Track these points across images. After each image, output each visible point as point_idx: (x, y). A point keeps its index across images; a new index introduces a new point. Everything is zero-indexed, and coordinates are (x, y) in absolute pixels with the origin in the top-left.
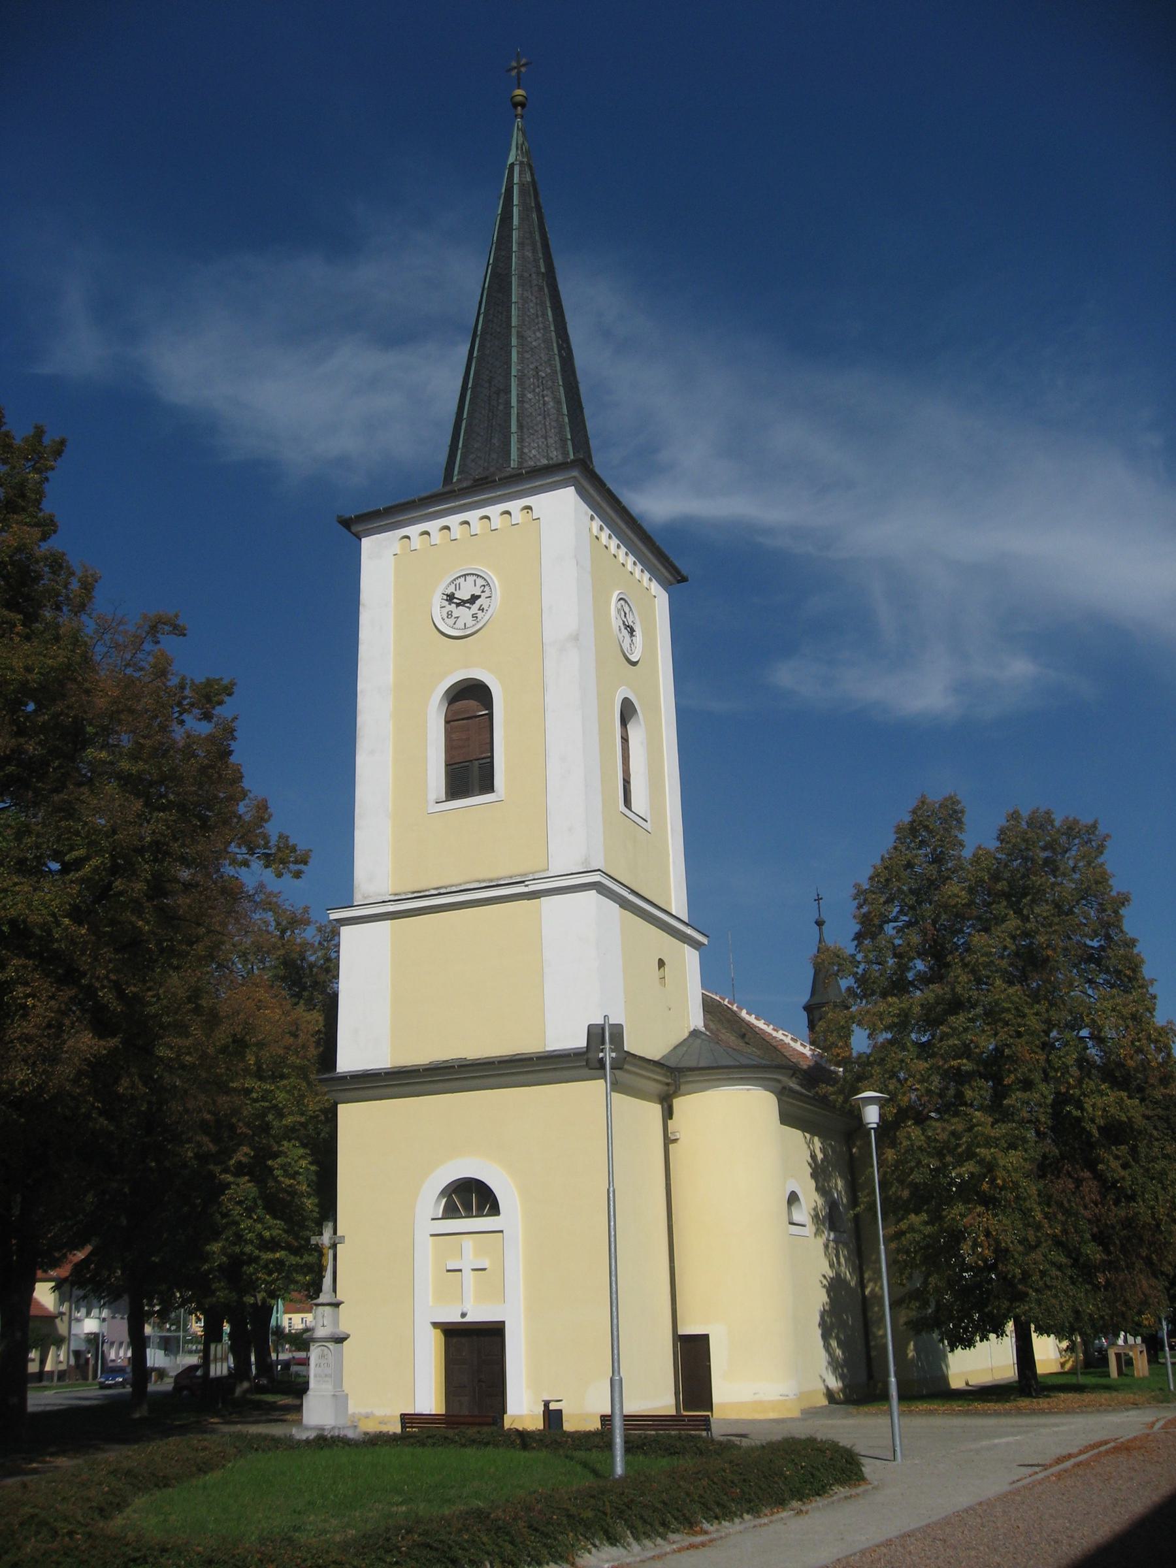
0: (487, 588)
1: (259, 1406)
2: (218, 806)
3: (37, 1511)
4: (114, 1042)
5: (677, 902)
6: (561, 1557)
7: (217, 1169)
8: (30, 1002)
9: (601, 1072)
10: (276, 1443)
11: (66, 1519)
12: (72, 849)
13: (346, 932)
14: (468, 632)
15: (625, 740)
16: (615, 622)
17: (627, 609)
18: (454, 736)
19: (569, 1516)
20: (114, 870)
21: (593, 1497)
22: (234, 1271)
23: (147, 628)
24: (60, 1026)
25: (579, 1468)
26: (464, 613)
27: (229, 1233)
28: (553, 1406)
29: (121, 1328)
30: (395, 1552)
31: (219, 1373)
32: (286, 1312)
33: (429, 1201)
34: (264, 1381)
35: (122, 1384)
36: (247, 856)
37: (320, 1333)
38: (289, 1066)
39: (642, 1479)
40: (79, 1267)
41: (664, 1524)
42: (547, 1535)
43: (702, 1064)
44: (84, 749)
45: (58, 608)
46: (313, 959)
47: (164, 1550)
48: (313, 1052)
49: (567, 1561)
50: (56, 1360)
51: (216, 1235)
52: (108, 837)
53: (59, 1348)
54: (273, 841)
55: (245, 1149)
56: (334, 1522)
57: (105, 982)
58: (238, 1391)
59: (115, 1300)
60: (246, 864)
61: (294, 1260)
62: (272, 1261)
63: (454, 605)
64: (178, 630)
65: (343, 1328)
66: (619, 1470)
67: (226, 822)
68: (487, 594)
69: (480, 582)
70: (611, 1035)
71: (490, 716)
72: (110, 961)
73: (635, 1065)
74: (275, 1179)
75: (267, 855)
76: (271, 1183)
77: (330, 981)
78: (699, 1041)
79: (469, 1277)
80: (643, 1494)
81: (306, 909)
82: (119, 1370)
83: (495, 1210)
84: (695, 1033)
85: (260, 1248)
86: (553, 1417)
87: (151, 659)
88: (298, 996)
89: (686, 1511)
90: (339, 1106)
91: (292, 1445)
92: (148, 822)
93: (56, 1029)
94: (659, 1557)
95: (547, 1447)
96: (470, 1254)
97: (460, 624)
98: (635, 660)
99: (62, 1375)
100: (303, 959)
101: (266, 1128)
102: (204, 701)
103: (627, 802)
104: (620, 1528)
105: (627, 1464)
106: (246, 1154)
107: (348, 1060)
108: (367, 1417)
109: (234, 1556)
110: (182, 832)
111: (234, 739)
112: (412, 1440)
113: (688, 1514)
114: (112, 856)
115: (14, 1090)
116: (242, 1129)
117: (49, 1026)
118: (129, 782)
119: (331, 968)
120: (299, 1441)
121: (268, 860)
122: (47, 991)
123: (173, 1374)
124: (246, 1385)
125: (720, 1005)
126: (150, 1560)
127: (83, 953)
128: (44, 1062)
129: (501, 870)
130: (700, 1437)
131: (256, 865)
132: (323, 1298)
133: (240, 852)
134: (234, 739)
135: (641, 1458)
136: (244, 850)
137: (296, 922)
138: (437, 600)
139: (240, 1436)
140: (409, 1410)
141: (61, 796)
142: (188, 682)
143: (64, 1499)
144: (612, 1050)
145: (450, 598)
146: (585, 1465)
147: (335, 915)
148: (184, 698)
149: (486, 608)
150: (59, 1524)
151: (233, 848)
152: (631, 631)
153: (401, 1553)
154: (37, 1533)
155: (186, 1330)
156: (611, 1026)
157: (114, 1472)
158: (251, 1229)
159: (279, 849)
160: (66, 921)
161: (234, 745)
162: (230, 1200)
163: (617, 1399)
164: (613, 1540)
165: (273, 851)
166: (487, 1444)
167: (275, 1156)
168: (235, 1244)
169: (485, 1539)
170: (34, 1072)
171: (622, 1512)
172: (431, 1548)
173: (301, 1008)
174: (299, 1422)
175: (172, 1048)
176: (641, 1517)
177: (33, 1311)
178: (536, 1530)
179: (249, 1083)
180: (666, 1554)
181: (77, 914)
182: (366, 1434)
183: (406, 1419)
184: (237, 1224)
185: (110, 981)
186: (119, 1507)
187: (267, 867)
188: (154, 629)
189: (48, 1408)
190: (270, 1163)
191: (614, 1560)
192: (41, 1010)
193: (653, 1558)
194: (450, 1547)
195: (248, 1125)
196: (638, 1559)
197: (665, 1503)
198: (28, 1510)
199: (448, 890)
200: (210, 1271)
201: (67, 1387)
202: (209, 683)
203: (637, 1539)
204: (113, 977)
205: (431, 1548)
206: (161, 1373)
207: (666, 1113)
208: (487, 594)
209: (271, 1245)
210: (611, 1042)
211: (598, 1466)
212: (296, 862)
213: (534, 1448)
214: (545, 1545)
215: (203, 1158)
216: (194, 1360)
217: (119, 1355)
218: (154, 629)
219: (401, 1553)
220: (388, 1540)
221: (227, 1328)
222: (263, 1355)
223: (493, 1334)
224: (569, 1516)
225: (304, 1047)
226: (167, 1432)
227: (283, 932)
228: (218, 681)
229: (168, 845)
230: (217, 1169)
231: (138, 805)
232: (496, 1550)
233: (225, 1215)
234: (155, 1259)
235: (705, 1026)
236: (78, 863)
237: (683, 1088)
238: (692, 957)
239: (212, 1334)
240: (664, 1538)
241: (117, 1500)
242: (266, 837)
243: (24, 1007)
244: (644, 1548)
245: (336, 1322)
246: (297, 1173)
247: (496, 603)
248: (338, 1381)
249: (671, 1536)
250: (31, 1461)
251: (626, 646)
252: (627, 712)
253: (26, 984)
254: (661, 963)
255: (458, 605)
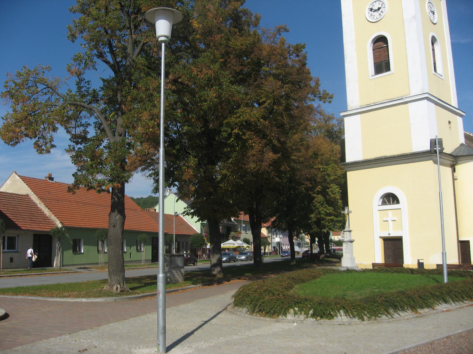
0: (383, 5)
1: (327, 261)
2: (304, 81)
3: (268, 288)
4: (279, 155)
5: (454, 102)
6: (429, 306)
7: (312, 193)
8: (253, 144)
9: (435, 154)
10: (334, 271)
11: (276, 290)
12: (261, 98)
13: (346, 119)
14: (378, 20)
15: (433, 50)
16: (428, 11)
17: (431, 6)
18: (376, 54)
19: (431, 294)
20: (274, 103)
21: (439, 288)
22: (318, 222)
23: (277, 31)
24: (263, 152)
25: (432, 280)
26: (376, 14)
27: (316, 211)
28: (421, 261)
29: (286, 240)
30: (377, 303)
31: (315, 252)
32: (333, 235)
33: (377, 200)
34: (328, 255)
35: (287, 256)
36: (314, 98)
37: (346, 240)
38: (332, 161)
39: (454, 283)
40: (273, 223)
41: (462, 298)
42: (425, 299)
43: (465, 154)
44: (261, 67)
45: (249, 26)
46: (335, 129)
47: (306, 300)
48: (339, 156)
49: (431, 307)
50: (269, 249)
51: (312, 212)
52: (271, 94)
53: (269, 246)
54: (321, 92)
55: (319, 187)
56: (356, 294)
57: (275, 138)
58: (321, 257)
59: (284, 231)
60: (313, 100)
61: (336, 219)
62: (330, 219)
63: (373, 12)
64: (286, 30)
65: (352, 238)
66: (446, 281)
67: (307, 86)
68: (383, 6)
69: (381, 3)
70: (438, 142)
71: (387, 46)
72: (276, 131)
73: (444, 156)
74: (329, 195)
75: (320, 97)
76: (328, 197)
77: (342, 136)
78: (463, 147)
79: (391, 223)
80: (455, 288)
81: (333, 114)
82: (287, 252)
83: (398, 202)
84: (462, 145)
85: (325, 216)
86: (421, 265)
87: (279, 40)
88: (332, 141)
89: (469, 294)
90: (348, 173)
91: (339, 272)
92: (283, 88)
93: (262, 152)
94: (462, 308)
95: (419, 273)
96: (390, 216)
97: (375, 17)
98: (435, 23)
99: (270, 253)
100: (333, 129)
101: (325, 180)
102: (296, 51)
103: (435, 70)
104: (448, 298)
105: (448, 279)
106: (320, 188)
107: (349, 158)
108: (360, 264)
109: (327, 302)
110: (294, 90)
111: (307, 59)
112: (376, 271)
113: (470, 295)
114: (273, 99)
115: (251, 171)
116: (318, 180)
117: (260, 151)
118: (276, 77)
119: (342, 132)
120: (341, 271)
121: (320, 98)
122: (258, 141)
123: (302, 253)
124: (323, 256)
125: (469, 136)
126: (302, 302)
127: (267, 129)
128: (259, 162)
129: (394, 96)
130: (471, 271)
131: (317, 100)
132: (346, 229)
133: (311, 96)
134: (307, 59)
135: (451, 277)
136: (313, 96)
137: (330, 118)
138: (367, 11)
139: (324, 269)
140: (374, 262)
141: (257, 83)
142: (291, 45)
143: (275, 285)
144: (439, 147)
145: (371, 10)
146: (433, 279)
147: (342, 114)
148: (290, 51)
149: (383, 11)
150: (275, 292)
151: (309, 95)
152: (434, 13)
153: (378, 303)
154: (268, 294)
155: (304, 241)
156: (438, 139)
157: (289, 278)
158: (322, 210)
159: (323, 95)
160: (262, 120)
161: (307, 62)
162: (316, 202)
163: (444, 258)
164: (446, 302)
165: (322, 95)
166: (400, 272)
167: (328, 188)
168: (318, 215)
169: (405, 300)
170: (257, 165)
171: (449, 293)
172: (388, 302)
173: (333, 144)
174: (341, 266)
175: (296, 156)
176: (455, 295)
177: (262, 236)
178: (421, 298)
179: (320, 166)
180: (463, 307)
181: (264, 118)
182: (362, 269)
183: (374, 265)
184: (318, 209)
185: (276, 137)
186: (291, 288)
187: (320, 100)
188: (279, 31)
189: (267, 262)
190: (327, 190)
191: (447, 308)
192: (257, 147)
193: (459, 308)
194: (394, 302)
195: (320, 179)
196: (455, 308)
197: (462, 291)
198: (265, 288)
199: (378, 103)
200: (311, 222)
201: (272, 256)
202: (297, 45)
203: (454, 302)
204: (277, 136)
205: (388, 302)
206: (298, 253)
207: (453, 170)
208: (383, 6)
209: (330, 215)
210: (439, 144)
211: (438, 279)
212: (329, 98)
213: (415, 274)
214: (424, 302)
215: (307, 189)
216: (307, 249)
217: (286, 247)
218: (279, 31)
219: (378, 303)
220: (374, 299)
221: (317, 239)
222: (327, 247)
223: (399, 240)
224: (431, 294)
225: (336, 154)
226: (302, 268)
227: (326, 122)
228: (300, 45)
229: (290, 94)
230: (312, 193)
231: (280, 83)
232: (409, 303)
233: (314, 206)
234: (295, 220)
235: (465, 142)
236: (264, 102)
237: (459, 162)
238: (459, 120)
239: (313, 241)
240: (462, 302)
241: (290, 286)
242: (319, 92)
243: (252, 146)
244: (456, 305)
245: (350, 236)
246: (335, 193)
247: (386, 10)
248: (352, 254)
249: (465, 301)
250: (264, 276)
251: (432, 18)
252: (434, 40)
253: (252, 139)
254: (450, 122)
255: (374, 11)
